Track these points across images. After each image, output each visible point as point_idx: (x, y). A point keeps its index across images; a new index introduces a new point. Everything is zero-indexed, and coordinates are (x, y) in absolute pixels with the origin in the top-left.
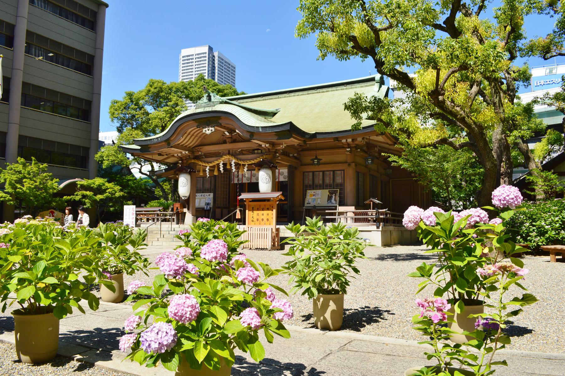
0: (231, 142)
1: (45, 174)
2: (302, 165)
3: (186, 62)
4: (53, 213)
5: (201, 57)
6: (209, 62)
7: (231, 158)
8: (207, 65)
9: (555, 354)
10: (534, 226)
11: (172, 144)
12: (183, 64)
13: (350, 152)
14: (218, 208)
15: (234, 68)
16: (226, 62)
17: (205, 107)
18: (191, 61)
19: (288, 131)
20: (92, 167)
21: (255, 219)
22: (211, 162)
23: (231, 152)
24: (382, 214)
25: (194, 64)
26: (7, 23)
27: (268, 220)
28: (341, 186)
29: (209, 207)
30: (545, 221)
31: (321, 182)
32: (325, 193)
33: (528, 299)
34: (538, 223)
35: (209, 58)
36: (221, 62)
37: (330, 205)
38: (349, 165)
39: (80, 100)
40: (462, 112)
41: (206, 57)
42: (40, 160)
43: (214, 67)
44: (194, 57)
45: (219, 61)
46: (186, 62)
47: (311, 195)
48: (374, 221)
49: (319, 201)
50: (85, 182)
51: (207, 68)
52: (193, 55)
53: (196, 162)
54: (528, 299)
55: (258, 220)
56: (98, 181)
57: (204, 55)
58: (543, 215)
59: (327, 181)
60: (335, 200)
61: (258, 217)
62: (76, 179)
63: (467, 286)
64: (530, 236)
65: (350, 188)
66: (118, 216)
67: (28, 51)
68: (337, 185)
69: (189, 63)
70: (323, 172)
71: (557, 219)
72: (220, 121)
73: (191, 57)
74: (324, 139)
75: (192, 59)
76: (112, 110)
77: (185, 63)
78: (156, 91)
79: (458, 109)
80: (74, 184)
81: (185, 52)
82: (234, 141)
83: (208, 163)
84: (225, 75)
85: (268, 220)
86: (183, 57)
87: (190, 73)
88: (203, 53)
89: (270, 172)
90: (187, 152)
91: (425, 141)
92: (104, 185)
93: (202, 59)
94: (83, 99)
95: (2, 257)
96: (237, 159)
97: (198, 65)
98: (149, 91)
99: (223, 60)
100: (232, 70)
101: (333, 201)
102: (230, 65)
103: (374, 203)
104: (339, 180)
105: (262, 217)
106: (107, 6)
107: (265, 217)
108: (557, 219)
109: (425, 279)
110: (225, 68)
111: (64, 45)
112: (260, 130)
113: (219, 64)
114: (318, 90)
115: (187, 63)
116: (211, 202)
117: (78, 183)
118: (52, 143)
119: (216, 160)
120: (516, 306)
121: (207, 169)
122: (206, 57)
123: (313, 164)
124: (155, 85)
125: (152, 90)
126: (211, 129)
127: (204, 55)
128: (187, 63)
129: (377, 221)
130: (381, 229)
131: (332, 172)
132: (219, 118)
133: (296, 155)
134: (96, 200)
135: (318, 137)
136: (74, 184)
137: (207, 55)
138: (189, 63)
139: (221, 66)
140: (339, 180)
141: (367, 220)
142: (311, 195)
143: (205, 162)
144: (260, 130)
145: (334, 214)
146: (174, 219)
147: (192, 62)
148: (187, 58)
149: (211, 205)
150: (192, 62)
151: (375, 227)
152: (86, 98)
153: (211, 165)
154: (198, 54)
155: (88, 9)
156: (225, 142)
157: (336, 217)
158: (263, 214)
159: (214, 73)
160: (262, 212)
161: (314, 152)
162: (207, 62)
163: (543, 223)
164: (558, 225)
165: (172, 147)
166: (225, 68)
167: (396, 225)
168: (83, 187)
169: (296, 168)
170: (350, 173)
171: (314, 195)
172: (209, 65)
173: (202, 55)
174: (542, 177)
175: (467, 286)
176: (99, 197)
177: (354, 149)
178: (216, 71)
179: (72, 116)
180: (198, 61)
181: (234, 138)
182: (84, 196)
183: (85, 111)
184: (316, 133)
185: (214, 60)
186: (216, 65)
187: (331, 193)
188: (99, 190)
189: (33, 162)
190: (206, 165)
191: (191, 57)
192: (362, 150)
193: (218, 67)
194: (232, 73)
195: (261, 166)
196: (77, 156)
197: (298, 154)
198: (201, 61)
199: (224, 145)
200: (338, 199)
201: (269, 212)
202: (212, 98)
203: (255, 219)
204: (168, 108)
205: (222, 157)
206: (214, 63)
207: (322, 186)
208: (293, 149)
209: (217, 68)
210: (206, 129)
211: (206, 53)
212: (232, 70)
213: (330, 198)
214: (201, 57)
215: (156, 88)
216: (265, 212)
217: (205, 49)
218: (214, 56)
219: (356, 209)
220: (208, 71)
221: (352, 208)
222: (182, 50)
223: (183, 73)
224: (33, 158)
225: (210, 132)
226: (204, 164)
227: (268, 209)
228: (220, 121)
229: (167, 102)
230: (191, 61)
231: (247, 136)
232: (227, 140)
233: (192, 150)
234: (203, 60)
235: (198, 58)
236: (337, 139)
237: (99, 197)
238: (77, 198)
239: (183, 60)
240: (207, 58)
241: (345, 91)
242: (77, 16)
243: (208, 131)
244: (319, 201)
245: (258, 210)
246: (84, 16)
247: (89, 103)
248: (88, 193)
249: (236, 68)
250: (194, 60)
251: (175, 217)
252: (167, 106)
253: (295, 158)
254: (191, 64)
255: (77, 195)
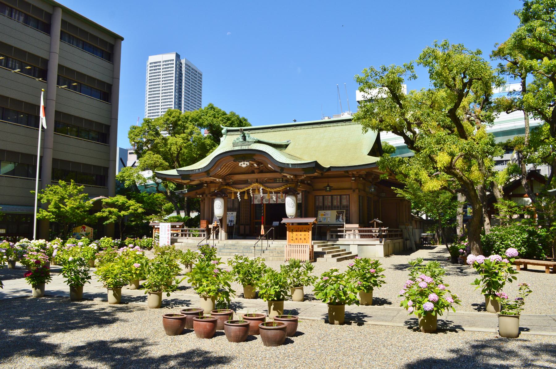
0: (259, 173)
1: (83, 195)
2: (314, 190)
3: (153, 68)
4: (84, 228)
5: (168, 64)
6: (176, 69)
7: (259, 185)
8: (174, 72)
9: (531, 314)
10: (503, 244)
11: (211, 174)
12: (150, 70)
13: (355, 180)
14: (242, 225)
15: (201, 75)
16: (193, 69)
17: (242, 146)
18: (158, 67)
19: (314, 167)
20: (111, 185)
21: (294, 239)
22: (242, 189)
23: (258, 180)
24: (384, 231)
25: (161, 70)
26: (42, 58)
27: (305, 239)
28: (347, 208)
29: (232, 224)
30: (511, 240)
31: (330, 204)
32: (334, 213)
33: (530, 291)
34: (506, 242)
35: (176, 65)
36: (188, 69)
37: (338, 223)
38: (354, 191)
39: (100, 125)
40: (460, 173)
41: (173, 64)
42: (78, 182)
43: (181, 74)
44: (162, 64)
45: (186, 68)
46: (153, 68)
47: (322, 215)
48: (378, 237)
49: (329, 220)
50: (109, 200)
51: (174, 75)
52: (160, 62)
53: (228, 188)
54: (530, 291)
55: (296, 239)
56: (121, 199)
57: (172, 62)
58: (509, 236)
59: (335, 203)
60: (342, 219)
61: (296, 237)
62: (101, 197)
63: (493, 287)
64: (501, 251)
65: (354, 209)
66: (148, 231)
67: (58, 83)
68: (344, 207)
69: (156, 69)
70: (332, 196)
71: (519, 239)
72: (254, 157)
73: (158, 64)
74: (336, 171)
75: (159, 66)
76: (132, 135)
77: (152, 70)
78: (174, 119)
79: (458, 171)
80: (99, 202)
81: (152, 59)
82: (261, 172)
83: (239, 189)
84: (192, 81)
85: (305, 239)
86: (150, 64)
87: (158, 80)
88: (171, 60)
89: (294, 198)
90: (220, 180)
91: (433, 188)
92: (127, 202)
93: (169, 66)
94: (103, 124)
95: (4, 268)
96: (265, 186)
97: (165, 71)
98: (168, 120)
99: (190, 67)
100: (199, 77)
101: (341, 220)
102: (196, 72)
103: (377, 222)
104: (345, 202)
105: (301, 237)
106: (122, 39)
107: (303, 238)
108: (519, 239)
109: (478, 286)
110: (192, 75)
111: (88, 76)
112: (290, 166)
113: (186, 71)
114: (322, 125)
115: (155, 70)
116: (234, 219)
117: (103, 200)
118: (79, 164)
119: (246, 187)
120: (527, 294)
121: (238, 194)
122: (173, 64)
123: (326, 190)
124: (173, 115)
125: (171, 119)
126: (246, 163)
127: (172, 62)
128: (155, 70)
129: (380, 237)
130: (383, 243)
131: (339, 197)
132: (254, 155)
133: (309, 182)
134: (120, 216)
135: (332, 170)
136: (99, 202)
137: (174, 62)
138: (156, 69)
139: (188, 73)
140: (345, 202)
141: (372, 237)
142: (322, 215)
143: (236, 188)
144: (290, 166)
145: (342, 231)
146: (204, 235)
147: (159, 69)
148: (154, 65)
149: (235, 222)
150: (159, 69)
151: (379, 242)
152: (106, 124)
153: (242, 191)
154: (165, 61)
155: (107, 42)
156: (253, 172)
157: (344, 234)
158: (301, 235)
159: (181, 80)
160: (300, 233)
161: (326, 180)
162: (174, 69)
163: (509, 243)
164: (519, 244)
165: (211, 177)
166: (192, 75)
167: (391, 238)
168: (109, 205)
169: (309, 192)
170: (355, 197)
171: (324, 215)
172: (176, 72)
173: (170, 62)
174: (506, 205)
175: (493, 287)
176: (123, 213)
177: (358, 178)
178: (183, 78)
179: (93, 139)
180: (165, 68)
181: (261, 169)
182: (110, 213)
183: (105, 133)
184: (331, 167)
185: (181, 67)
186: (183, 72)
187: (339, 213)
188: (122, 207)
189: (72, 184)
190: (238, 191)
191: (158, 64)
192: (363, 179)
193: (186, 74)
194: (199, 80)
195: (287, 193)
196: (98, 177)
197: (311, 181)
198: (168, 68)
199: (253, 175)
200: (344, 218)
201: (306, 233)
202: (247, 138)
203: (294, 239)
204: (185, 135)
205: (251, 184)
206: (181, 70)
207: (331, 208)
208: (312, 181)
209: (184, 75)
210: (242, 163)
211: (173, 60)
212: (199, 77)
213: (338, 218)
214: (168, 64)
215: (174, 117)
216: (303, 233)
217: (173, 56)
218: (181, 63)
219: (360, 226)
220: (176, 78)
221: (357, 226)
222: (150, 57)
223: (150, 80)
224: (72, 181)
225: (245, 165)
226: (235, 190)
227: (305, 231)
228: (254, 157)
229: (184, 130)
230: (158, 67)
231: (278, 170)
232: (256, 171)
233: (224, 178)
234: (170, 67)
235: (166, 65)
236: (347, 172)
237: (123, 213)
238: (105, 215)
239: (150, 67)
240: (174, 65)
241: (344, 126)
242: (78, 40)
243: (244, 164)
244: (329, 220)
245: (297, 231)
246: (103, 49)
247: (108, 127)
248: (113, 209)
249: (203, 75)
250: (161, 67)
251: (205, 233)
252: (184, 133)
253: (308, 184)
254: (158, 71)
255: (104, 212)
